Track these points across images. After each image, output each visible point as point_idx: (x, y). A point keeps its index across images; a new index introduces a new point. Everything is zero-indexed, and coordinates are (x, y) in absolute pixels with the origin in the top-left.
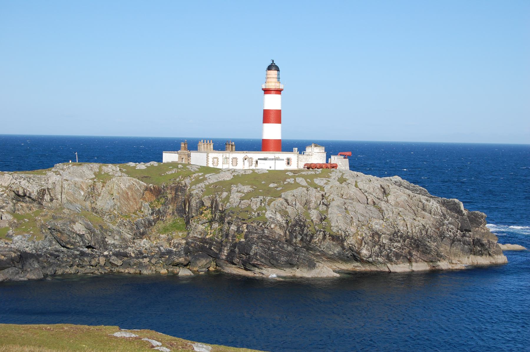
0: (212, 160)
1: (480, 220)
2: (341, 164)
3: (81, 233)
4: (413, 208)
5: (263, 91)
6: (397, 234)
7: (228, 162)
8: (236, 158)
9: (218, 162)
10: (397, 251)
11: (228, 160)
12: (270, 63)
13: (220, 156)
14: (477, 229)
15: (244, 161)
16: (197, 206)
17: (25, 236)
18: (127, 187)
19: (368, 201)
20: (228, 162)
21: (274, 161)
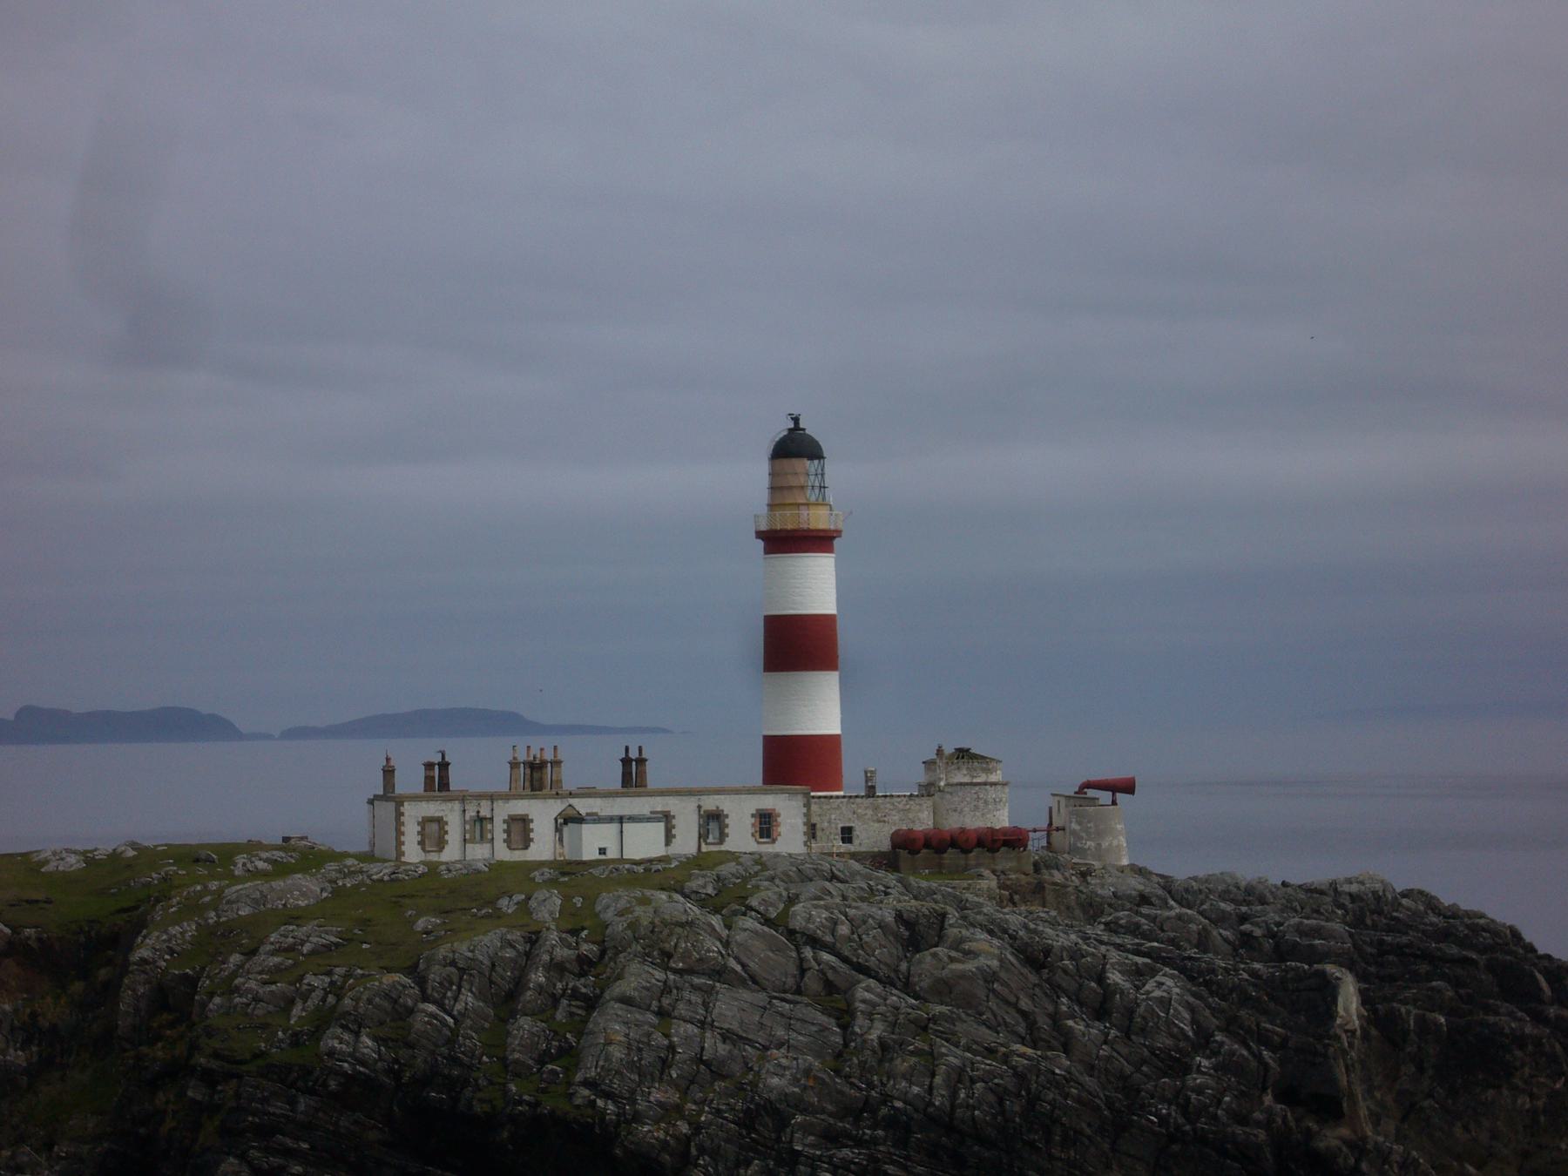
6: (874, 1112)
7: (489, 836)
9: (404, 848)
11: (489, 826)
12: (782, 427)
13: (452, 810)
14: (1490, 1093)
15: (558, 830)
20: (489, 836)
21: (614, 827)
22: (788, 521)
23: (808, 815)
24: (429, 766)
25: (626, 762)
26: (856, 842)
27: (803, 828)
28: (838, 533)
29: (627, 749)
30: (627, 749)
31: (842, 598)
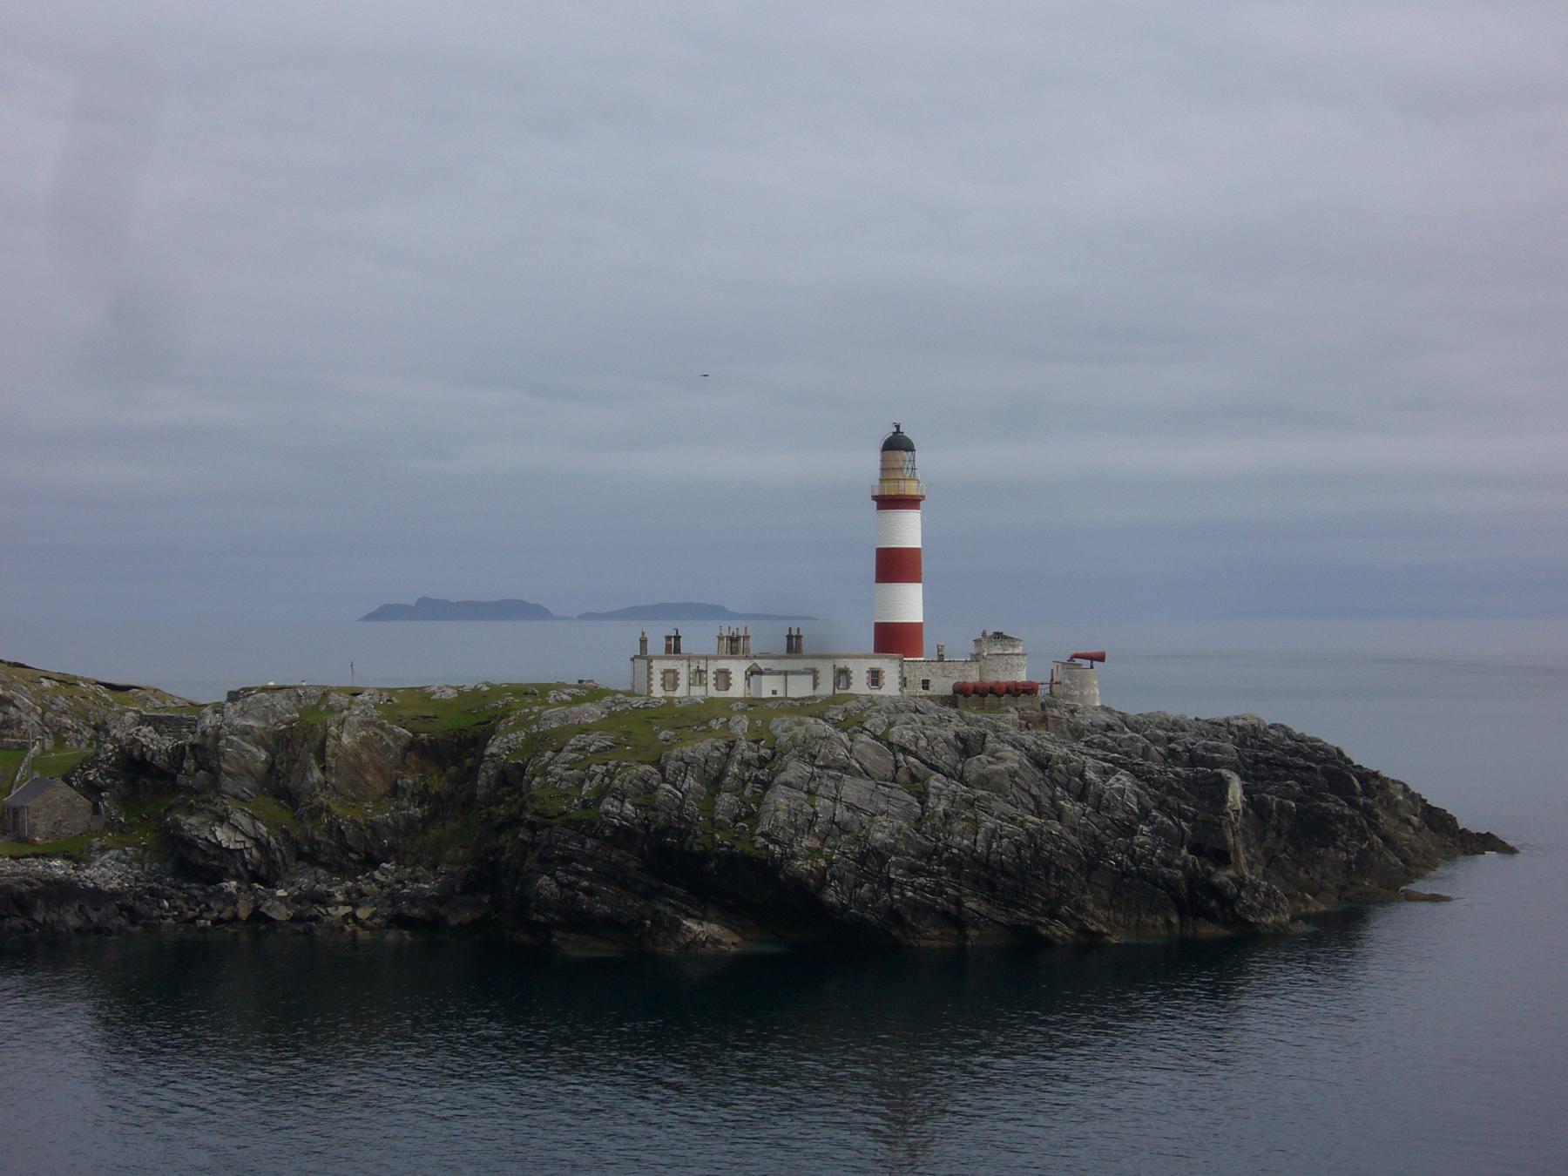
0: (662, 676)
1: (1334, 828)
2: (1069, 682)
3: (231, 847)
4: (1034, 791)
5: (875, 503)
6: (940, 856)
8: (674, 672)
10: (918, 898)
11: (705, 676)
15: (747, 678)
16: (489, 784)
17: (126, 853)
18: (358, 741)
19: (897, 772)
22: (891, 490)
23: (901, 672)
24: (668, 638)
25: (790, 637)
26: (931, 689)
27: (898, 680)
28: (923, 497)
29: (790, 630)
30: (790, 630)
31: (922, 545)
